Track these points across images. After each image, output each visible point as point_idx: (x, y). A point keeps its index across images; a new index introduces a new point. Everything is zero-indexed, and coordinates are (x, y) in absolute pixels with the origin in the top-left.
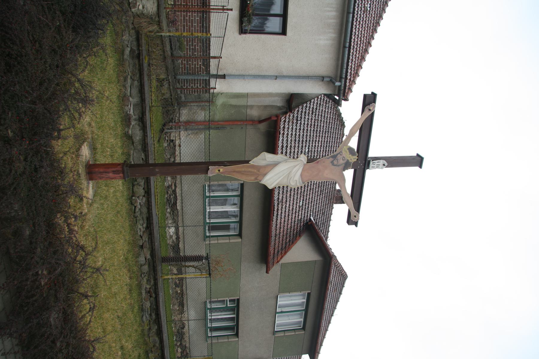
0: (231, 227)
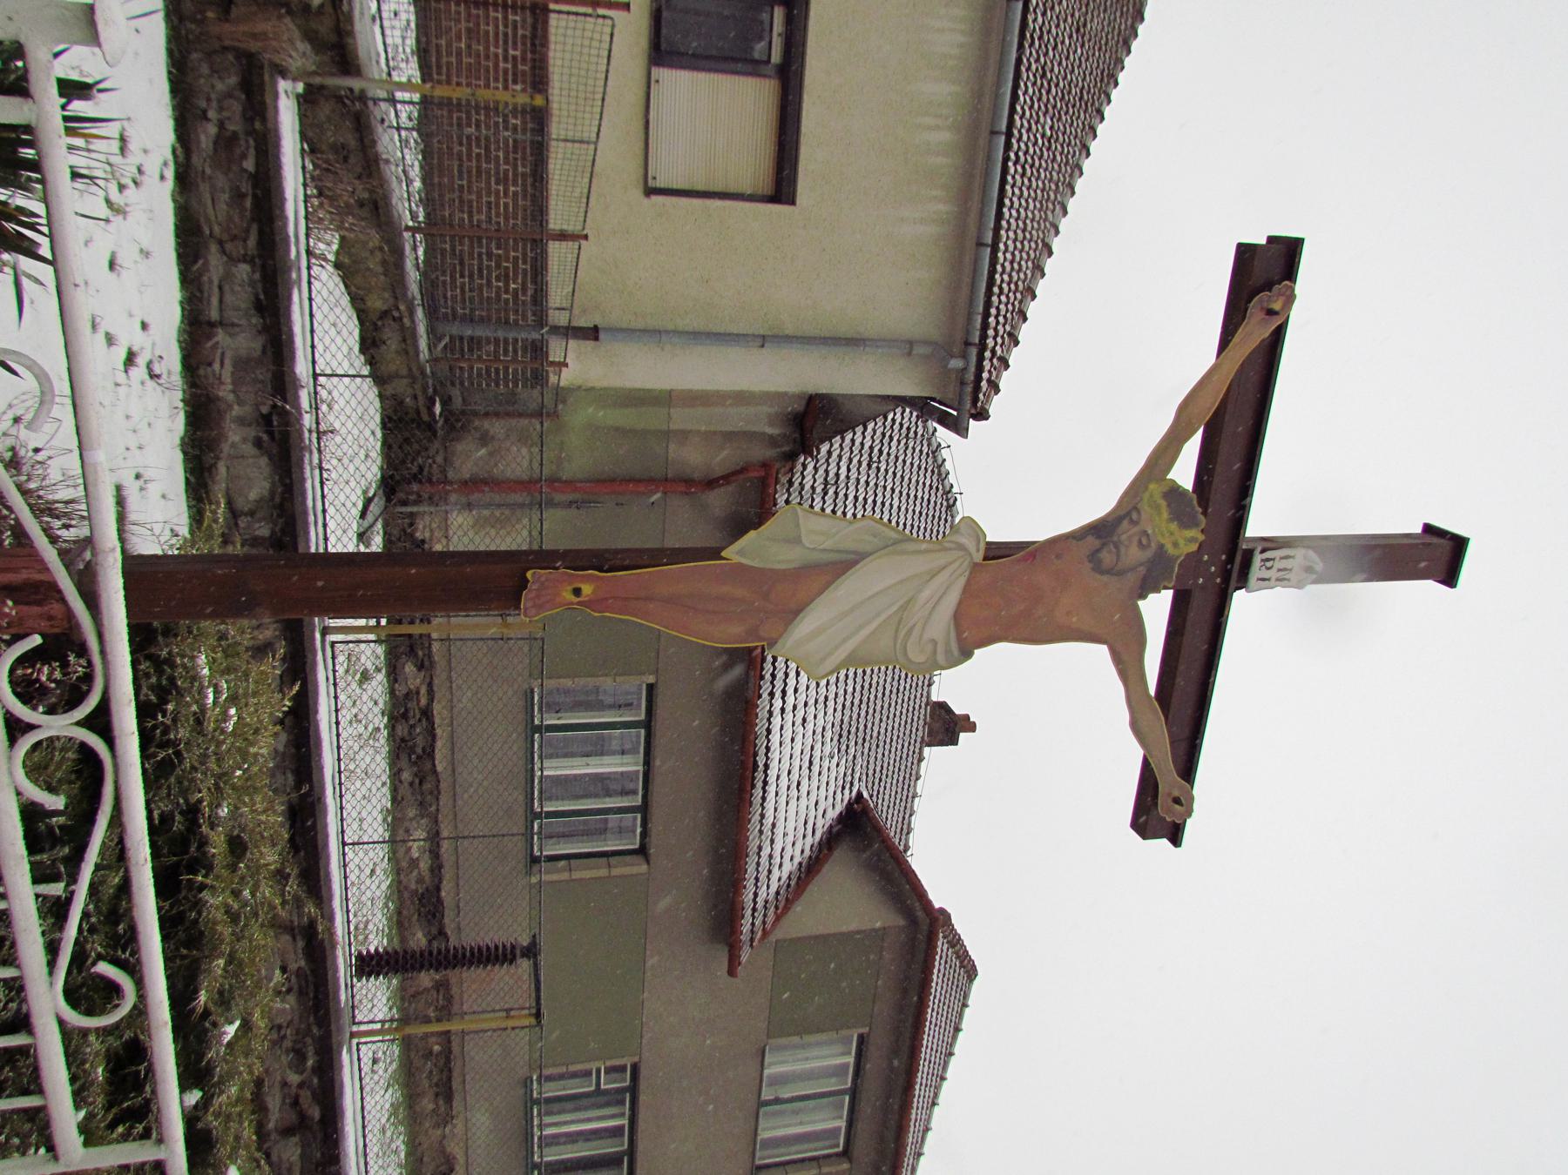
0: (610, 825)
